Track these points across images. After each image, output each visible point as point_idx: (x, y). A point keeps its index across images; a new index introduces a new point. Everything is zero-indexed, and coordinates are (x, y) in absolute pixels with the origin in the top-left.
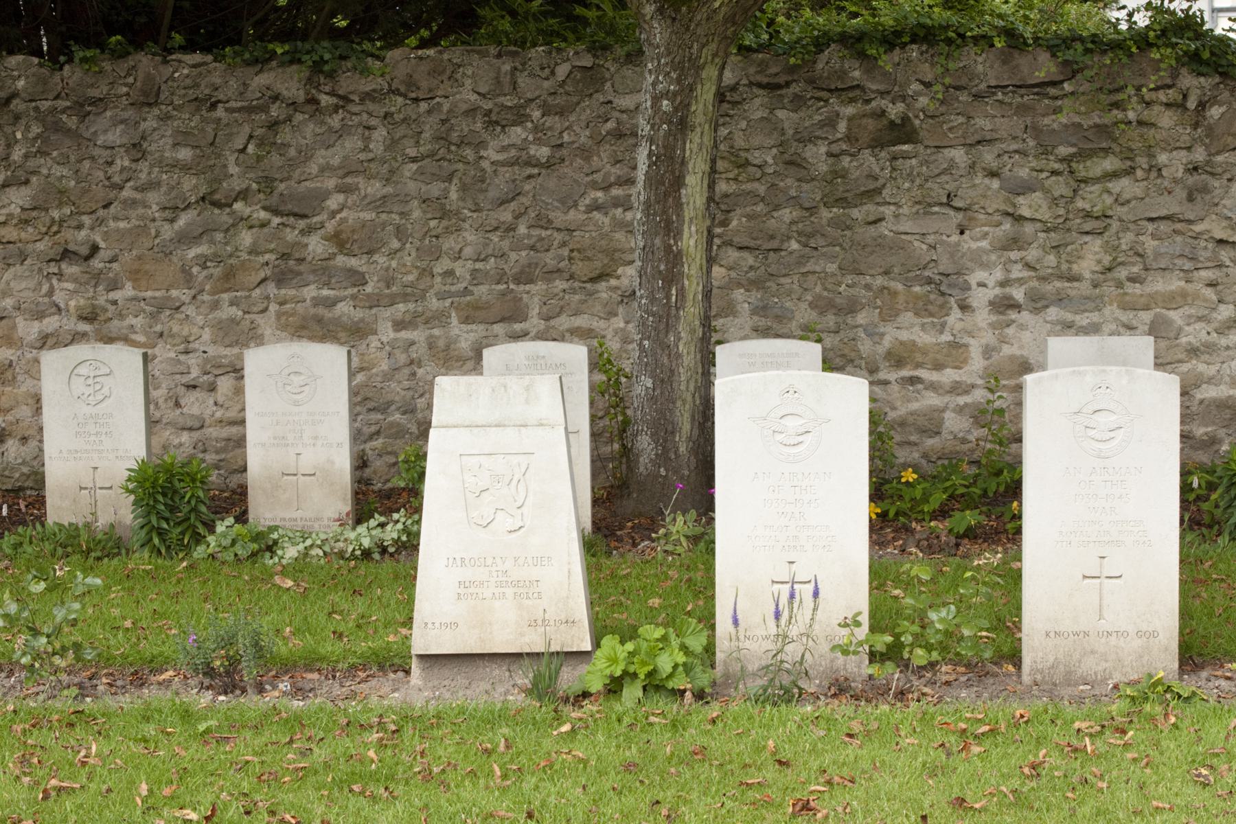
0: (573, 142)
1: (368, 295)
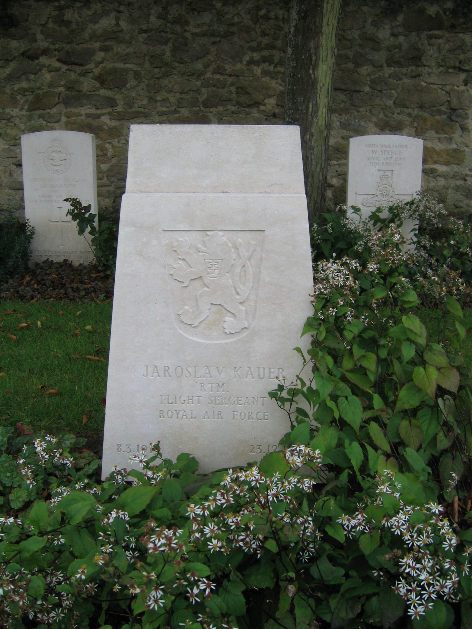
0: (240, 22)
1: (119, 113)
